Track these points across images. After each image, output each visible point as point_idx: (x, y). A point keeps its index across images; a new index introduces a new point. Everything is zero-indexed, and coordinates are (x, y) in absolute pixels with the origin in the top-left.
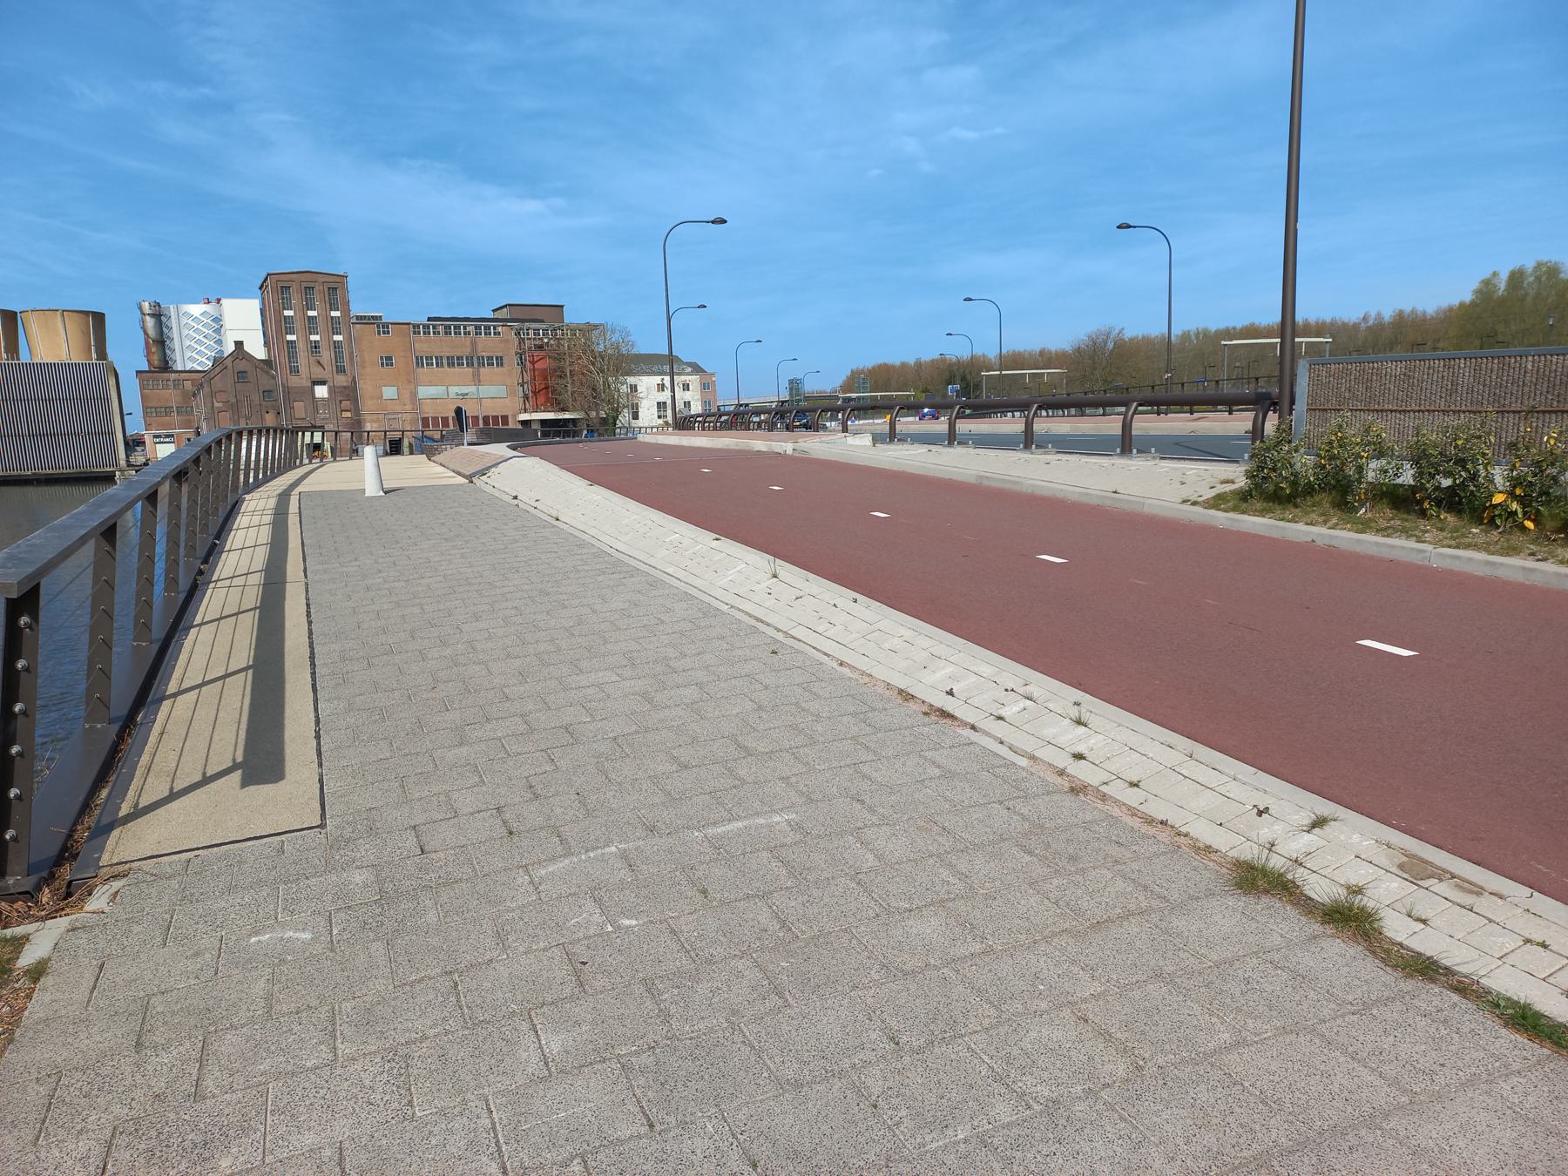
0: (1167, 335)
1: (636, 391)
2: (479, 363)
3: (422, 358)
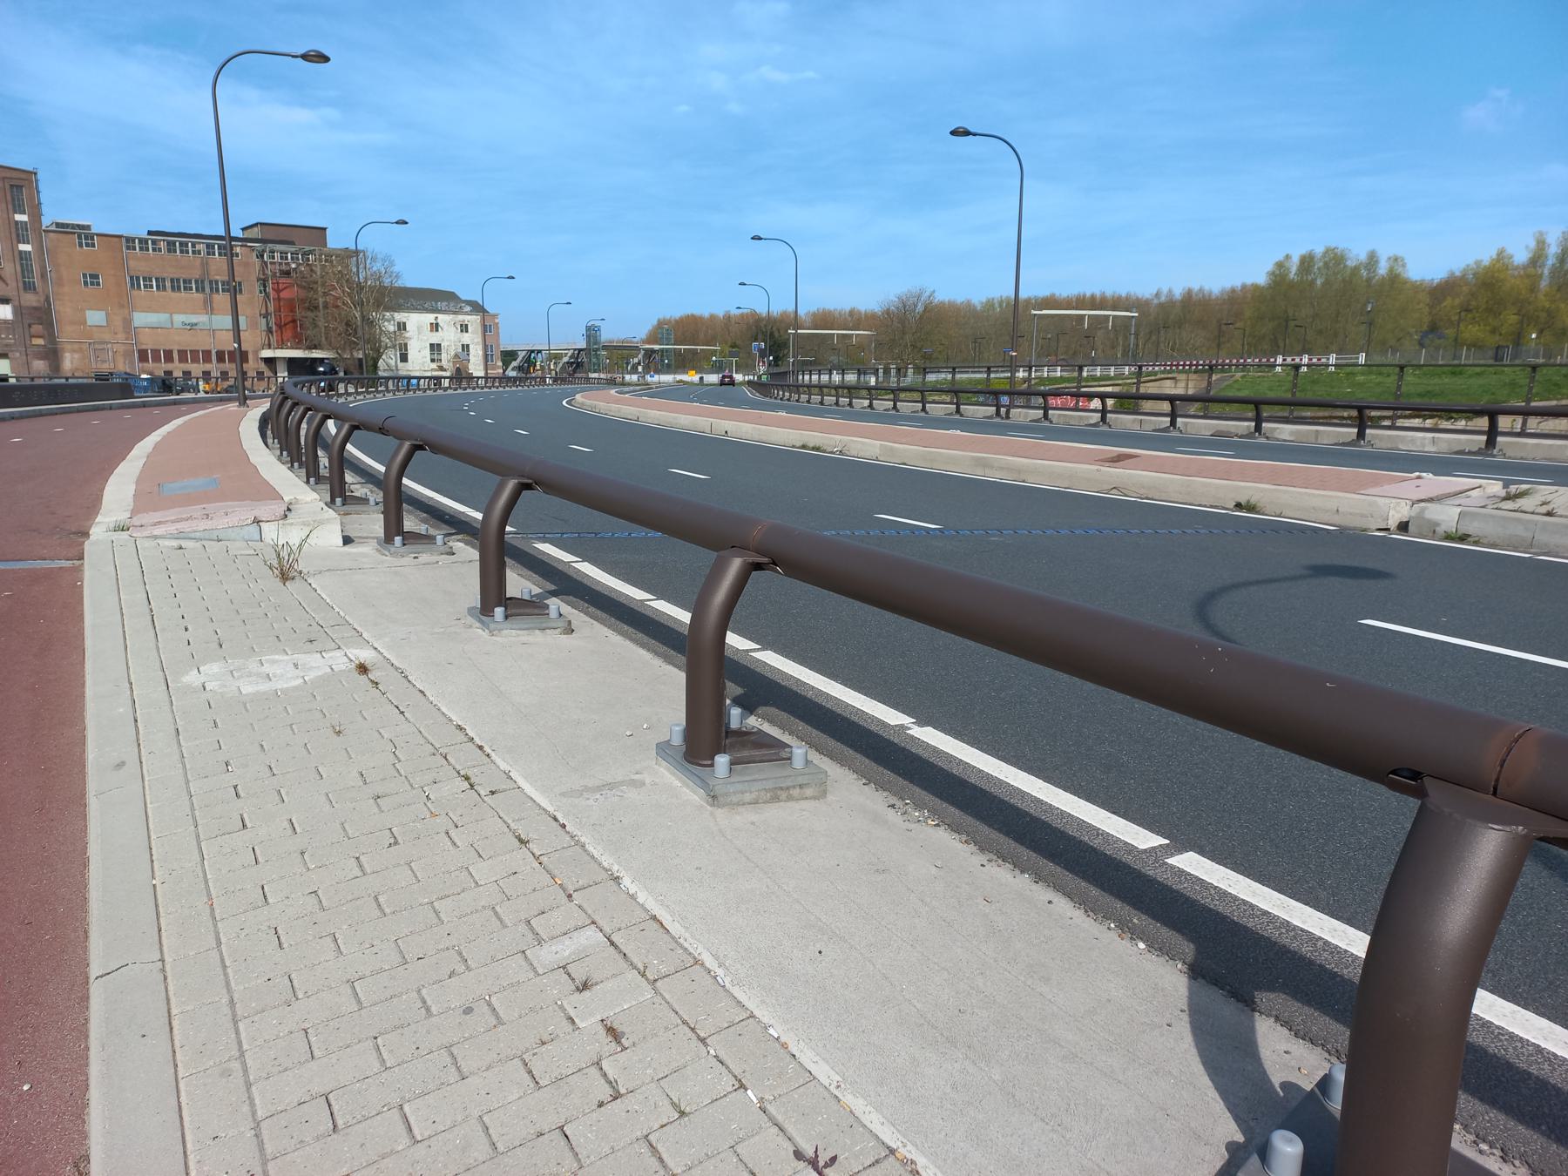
0: (1013, 297)
1: (405, 329)
2: (211, 289)
3: (138, 279)
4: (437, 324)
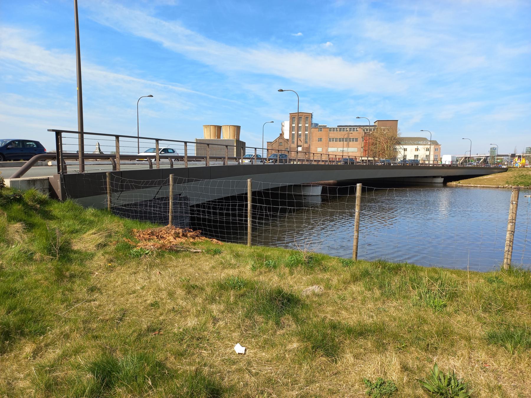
2: (349, 140)
3: (331, 139)
4: (418, 149)
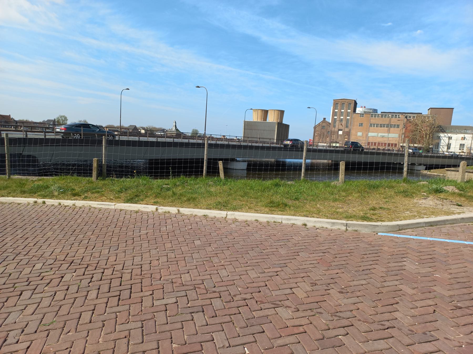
3: (372, 124)
